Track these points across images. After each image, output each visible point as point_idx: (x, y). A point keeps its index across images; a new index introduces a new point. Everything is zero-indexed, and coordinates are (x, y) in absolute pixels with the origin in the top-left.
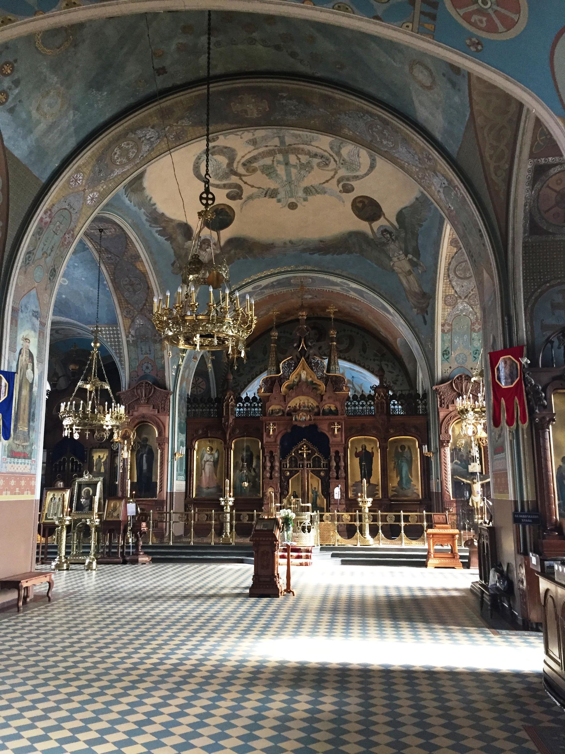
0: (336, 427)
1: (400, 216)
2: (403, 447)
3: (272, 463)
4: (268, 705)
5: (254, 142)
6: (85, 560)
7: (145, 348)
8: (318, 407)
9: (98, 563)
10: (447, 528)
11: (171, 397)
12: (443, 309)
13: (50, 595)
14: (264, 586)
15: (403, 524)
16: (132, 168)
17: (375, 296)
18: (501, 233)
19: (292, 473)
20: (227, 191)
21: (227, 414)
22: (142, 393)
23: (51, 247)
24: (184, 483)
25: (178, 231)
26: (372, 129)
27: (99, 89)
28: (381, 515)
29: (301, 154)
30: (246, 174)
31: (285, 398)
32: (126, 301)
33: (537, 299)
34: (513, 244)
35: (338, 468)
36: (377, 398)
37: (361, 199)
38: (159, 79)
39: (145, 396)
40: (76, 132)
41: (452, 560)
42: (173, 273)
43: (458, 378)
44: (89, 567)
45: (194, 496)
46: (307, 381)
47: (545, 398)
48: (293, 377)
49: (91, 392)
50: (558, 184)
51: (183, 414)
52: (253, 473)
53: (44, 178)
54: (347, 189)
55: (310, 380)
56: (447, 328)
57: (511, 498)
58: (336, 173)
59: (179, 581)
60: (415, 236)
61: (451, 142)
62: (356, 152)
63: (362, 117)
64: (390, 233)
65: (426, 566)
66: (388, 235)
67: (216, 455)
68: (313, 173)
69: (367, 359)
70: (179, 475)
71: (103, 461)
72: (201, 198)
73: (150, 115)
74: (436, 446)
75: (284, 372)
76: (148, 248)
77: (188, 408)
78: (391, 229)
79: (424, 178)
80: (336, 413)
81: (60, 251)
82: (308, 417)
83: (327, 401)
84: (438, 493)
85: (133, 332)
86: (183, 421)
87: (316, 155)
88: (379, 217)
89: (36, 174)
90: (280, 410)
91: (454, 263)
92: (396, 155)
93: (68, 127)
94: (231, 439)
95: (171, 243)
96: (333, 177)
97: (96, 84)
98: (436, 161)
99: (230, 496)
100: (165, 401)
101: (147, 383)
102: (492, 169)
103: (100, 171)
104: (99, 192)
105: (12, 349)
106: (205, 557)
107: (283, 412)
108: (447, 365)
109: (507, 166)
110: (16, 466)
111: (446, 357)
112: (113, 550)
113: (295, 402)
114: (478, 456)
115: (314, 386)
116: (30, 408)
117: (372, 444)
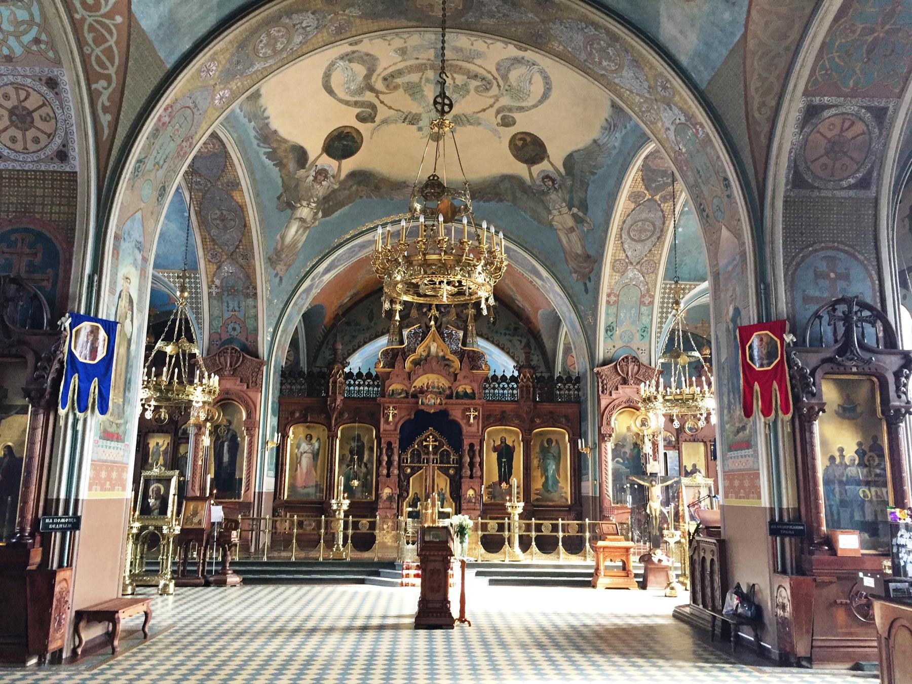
0: (473, 414)
1: (569, 162)
2: (549, 441)
3: (389, 457)
5: (403, 52)
6: (158, 582)
7: (233, 304)
8: (450, 388)
9: (176, 585)
10: (619, 540)
12: (611, 276)
13: (147, 630)
14: (434, 614)
15: (561, 535)
16: (276, 63)
18: (757, 182)
20: (358, 110)
21: (334, 393)
22: (226, 363)
23: (164, 157)
24: (273, 480)
25: (291, 156)
26: (591, 45)
29: (458, 73)
32: (213, 240)
33: (798, 264)
34: (773, 198)
35: (472, 465)
36: (522, 380)
37: (522, 136)
39: (231, 366)
41: (626, 579)
42: (279, 209)
43: (623, 359)
44: (164, 592)
45: (286, 497)
46: (437, 356)
47: (814, 384)
48: (420, 350)
49: (171, 357)
50: (830, 130)
52: (364, 469)
53: (170, 63)
54: (507, 122)
55: (441, 354)
56: (613, 298)
57: (765, 502)
59: (201, 609)
60: (584, 185)
61: (702, 68)
62: (528, 78)
63: (582, 29)
64: (553, 180)
65: (594, 586)
66: (550, 183)
67: (316, 445)
68: (468, 98)
70: (269, 470)
71: (162, 449)
72: (435, 103)
76: (251, 172)
77: (282, 384)
78: (555, 175)
79: (649, 111)
80: (472, 396)
82: (439, 401)
84: (595, 497)
85: (217, 282)
87: (476, 77)
88: (542, 159)
89: (162, 55)
92: (617, 81)
94: (337, 425)
95: (280, 170)
96: (491, 106)
99: (344, 498)
101: (233, 349)
102: (756, 105)
103: (238, 62)
104: (231, 90)
105: (112, 291)
107: (407, 393)
109: (774, 103)
110: (108, 451)
112: (188, 568)
113: (421, 381)
114: (651, 453)
116: (127, 372)
117: (512, 435)
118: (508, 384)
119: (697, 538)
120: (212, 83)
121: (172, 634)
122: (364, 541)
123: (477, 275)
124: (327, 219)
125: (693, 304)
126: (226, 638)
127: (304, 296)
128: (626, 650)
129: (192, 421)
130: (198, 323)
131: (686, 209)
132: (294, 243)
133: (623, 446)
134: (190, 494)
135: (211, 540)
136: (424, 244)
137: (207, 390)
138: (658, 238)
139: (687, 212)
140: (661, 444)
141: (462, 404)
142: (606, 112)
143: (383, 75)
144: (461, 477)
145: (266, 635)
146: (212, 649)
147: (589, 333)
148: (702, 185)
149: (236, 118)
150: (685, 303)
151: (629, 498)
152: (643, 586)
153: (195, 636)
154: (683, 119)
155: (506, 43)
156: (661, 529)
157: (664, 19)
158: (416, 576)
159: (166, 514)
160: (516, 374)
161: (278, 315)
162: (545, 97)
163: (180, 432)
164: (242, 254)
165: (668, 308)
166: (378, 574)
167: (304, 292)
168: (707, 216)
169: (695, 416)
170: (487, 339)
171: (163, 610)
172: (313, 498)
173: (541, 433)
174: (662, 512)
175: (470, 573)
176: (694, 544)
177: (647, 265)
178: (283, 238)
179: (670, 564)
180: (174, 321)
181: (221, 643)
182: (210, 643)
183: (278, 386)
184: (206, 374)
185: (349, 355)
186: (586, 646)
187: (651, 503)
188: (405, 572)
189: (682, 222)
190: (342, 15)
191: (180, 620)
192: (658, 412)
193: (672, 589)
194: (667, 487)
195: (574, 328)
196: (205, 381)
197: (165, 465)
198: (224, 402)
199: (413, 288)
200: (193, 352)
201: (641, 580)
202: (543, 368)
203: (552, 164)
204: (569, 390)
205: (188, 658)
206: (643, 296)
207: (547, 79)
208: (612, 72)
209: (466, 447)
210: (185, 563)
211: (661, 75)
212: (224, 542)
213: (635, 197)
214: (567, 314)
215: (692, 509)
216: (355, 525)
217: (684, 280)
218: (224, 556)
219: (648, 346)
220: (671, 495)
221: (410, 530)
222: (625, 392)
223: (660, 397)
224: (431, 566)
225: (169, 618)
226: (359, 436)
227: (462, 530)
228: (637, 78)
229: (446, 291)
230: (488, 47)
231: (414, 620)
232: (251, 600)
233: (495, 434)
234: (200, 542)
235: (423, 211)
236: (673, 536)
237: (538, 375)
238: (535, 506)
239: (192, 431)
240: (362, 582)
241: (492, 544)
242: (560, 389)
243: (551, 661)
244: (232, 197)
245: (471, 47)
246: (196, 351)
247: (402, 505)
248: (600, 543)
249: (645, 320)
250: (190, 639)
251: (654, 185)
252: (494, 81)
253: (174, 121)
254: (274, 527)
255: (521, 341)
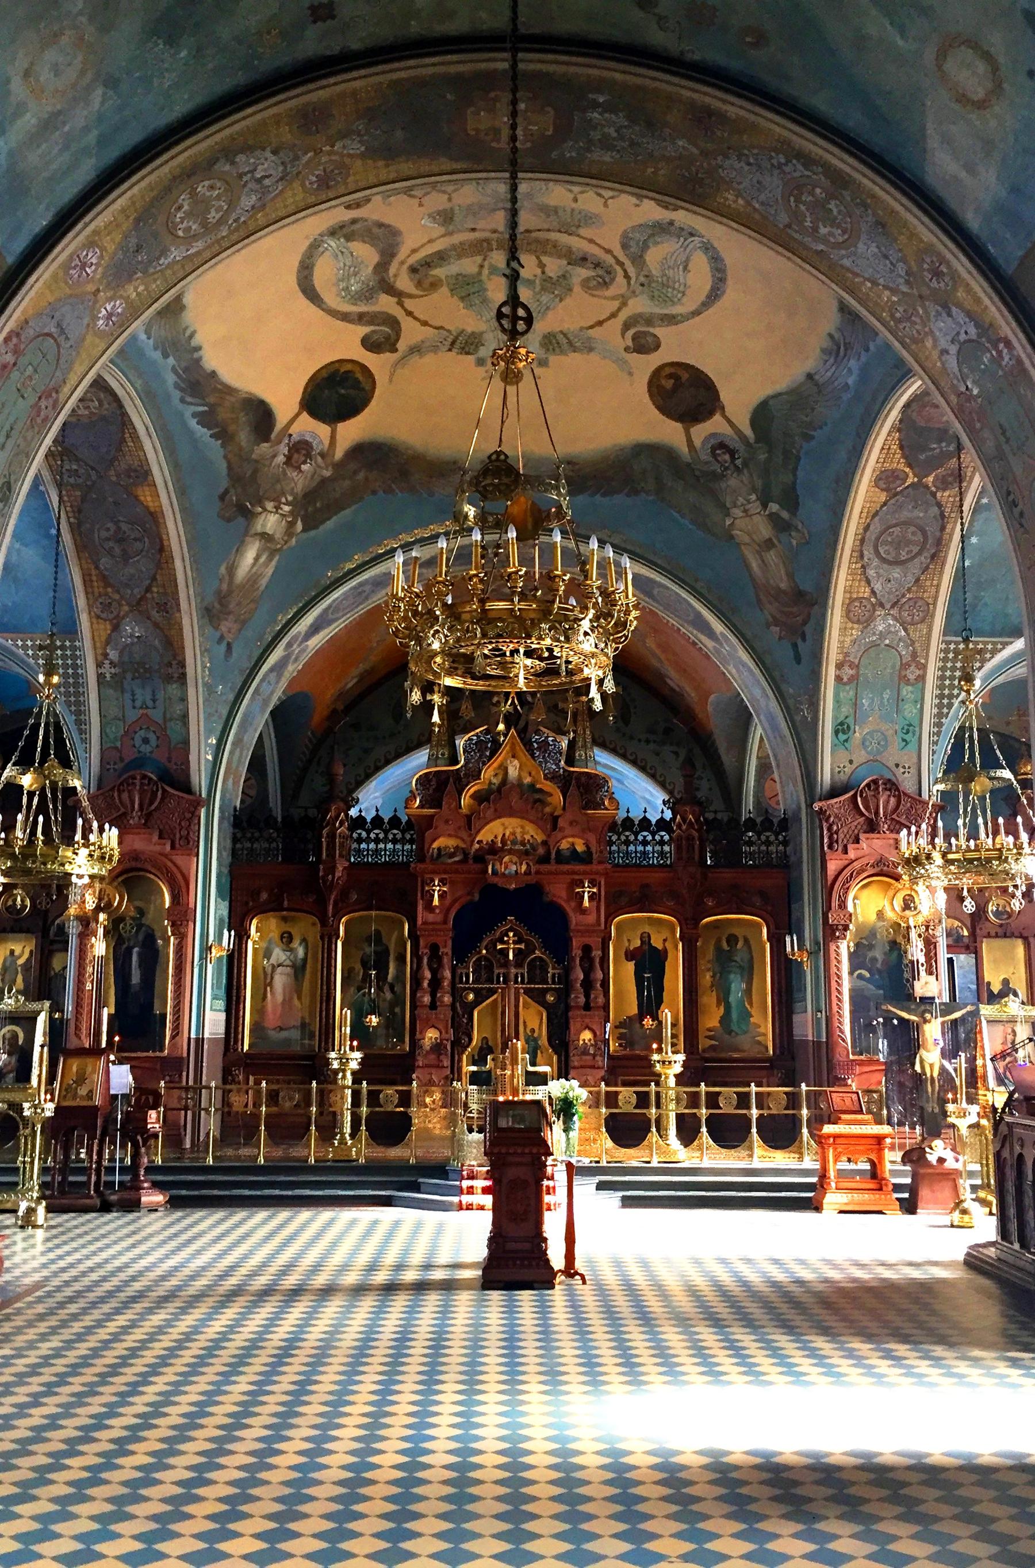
1: (762, 414)
2: (732, 940)
3: (434, 972)
4: (293, 1526)
5: (446, 217)
7: (143, 695)
8: (545, 843)
9: (49, 1210)
11: (203, 812)
12: (843, 630)
14: (517, 1261)
16: (209, 247)
17: (684, 595)
19: (481, 996)
20: (363, 330)
21: (331, 854)
25: (243, 418)
27: (171, 41)
28: (707, 1093)
29: (551, 255)
30: (414, 291)
31: (470, 823)
35: (588, 985)
36: (679, 826)
37: (672, 370)
38: (312, 32)
40: (103, 141)
41: (877, 1196)
42: (223, 518)
43: (868, 785)
44: (28, 1222)
45: (246, 1047)
46: (520, 784)
49: (31, 795)
51: (225, 854)
52: (388, 995)
55: (528, 780)
56: (848, 672)
58: (624, 304)
59: (94, 1253)
60: (791, 460)
63: (780, 166)
64: (732, 453)
65: (818, 1208)
66: (727, 457)
67: (301, 952)
68: (568, 301)
69: (632, 738)
70: (215, 997)
71: (21, 961)
72: (500, 315)
73: (277, 120)
74: (816, 936)
75: (467, 761)
77: (235, 840)
78: (736, 444)
80: (586, 858)
81: (25, 438)
82: (524, 867)
83: (567, 832)
84: (819, 1043)
85: (113, 655)
86: (226, 871)
87: (584, 260)
88: (711, 414)
90: (457, 848)
91: (876, 527)
92: (846, 262)
93: (86, 129)
95: (223, 446)
96: (613, 315)
97: (166, 28)
98: (955, 276)
99: (352, 1049)
100: (190, 820)
101: (144, 777)
106: (267, 1192)
108: (843, 756)
111: (842, 737)
112: (71, 1179)
113: (492, 831)
115: (537, 796)
117: (663, 929)
118: (653, 834)
119: (1008, 1119)
120: (90, 288)
121: (40, 1300)
122: (390, 1128)
123: (581, 638)
124: (313, 533)
125: (1001, 680)
126: (138, 1307)
127: (273, 676)
128: (873, 1326)
129: (73, 910)
130: (81, 732)
131: (985, 501)
132: (253, 579)
133: (871, 947)
134: (73, 1043)
135: (111, 1127)
136: (481, 581)
137: (96, 854)
138: (933, 557)
139: (988, 507)
140: (942, 943)
141: (568, 873)
142: (830, 321)
143: (412, 260)
144: (568, 1008)
145: (210, 1301)
146: (112, 1327)
147: (804, 735)
148: (1010, 457)
149: (141, 353)
150: (984, 680)
151: (883, 1044)
152: (910, 1207)
153: (82, 1303)
154: (973, 331)
155: (639, 197)
156: (943, 1102)
157: (933, 142)
158: (485, 1191)
159: (28, 1079)
160: (668, 815)
161: (225, 712)
162: (714, 295)
163: (53, 930)
164: (157, 604)
165: (952, 687)
166: (416, 1188)
167: (272, 670)
168: (1022, 514)
169: (1004, 890)
170: (614, 751)
171: (25, 1256)
172: (297, 1048)
173: (716, 925)
174: (943, 1069)
175: (585, 1188)
176: (1003, 1129)
177: (913, 609)
178: (231, 570)
179: (959, 1166)
180: (35, 728)
181: (129, 1315)
182: (109, 1317)
183: (229, 843)
184: (95, 825)
185: (360, 783)
186: (798, 1320)
187: (923, 1052)
188: (465, 1184)
189: (977, 526)
190: (329, 153)
191: (55, 1274)
192: (934, 883)
193: (964, 1212)
194: (955, 1022)
195: (775, 728)
196: (93, 838)
197: (24, 992)
198: (129, 875)
199: (461, 663)
200: (71, 784)
201: (906, 1195)
202: (718, 804)
203: (729, 421)
204: (768, 843)
205: (69, 1345)
206: (905, 666)
207: (717, 262)
208: (838, 246)
209: (577, 953)
210: (65, 1168)
211: (929, 249)
212: (134, 1130)
213: (886, 479)
214: (763, 703)
215: (1001, 1065)
216: (373, 1098)
217: (981, 634)
218: (136, 1156)
219: (915, 760)
220: (962, 1038)
221: (474, 1107)
222: (871, 846)
223: (937, 856)
224: (512, 1173)
225: (35, 1270)
226: (378, 933)
227: (566, 1108)
228: (886, 257)
229: (523, 668)
230: (606, 205)
231: (480, 1273)
232: (184, 1237)
233: (630, 928)
234: (91, 1130)
235: (482, 519)
236: (964, 1116)
237: (710, 816)
238: (707, 1060)
239: (73, 929)
240: (387, 1202)
241: (628, 1130)
242: (750, 843)
243: (734, 1348)
244: (136, 497)
245: (574, 205)
246: (76, 783)
247: (460, 1060)
248: (828, 1129)
249: (909, 711)
250: (73, 1308)
251: (922, 457)
252: (618, 268)
253: (23, 361)
254: (226, 1102)
255: (676, 754)
